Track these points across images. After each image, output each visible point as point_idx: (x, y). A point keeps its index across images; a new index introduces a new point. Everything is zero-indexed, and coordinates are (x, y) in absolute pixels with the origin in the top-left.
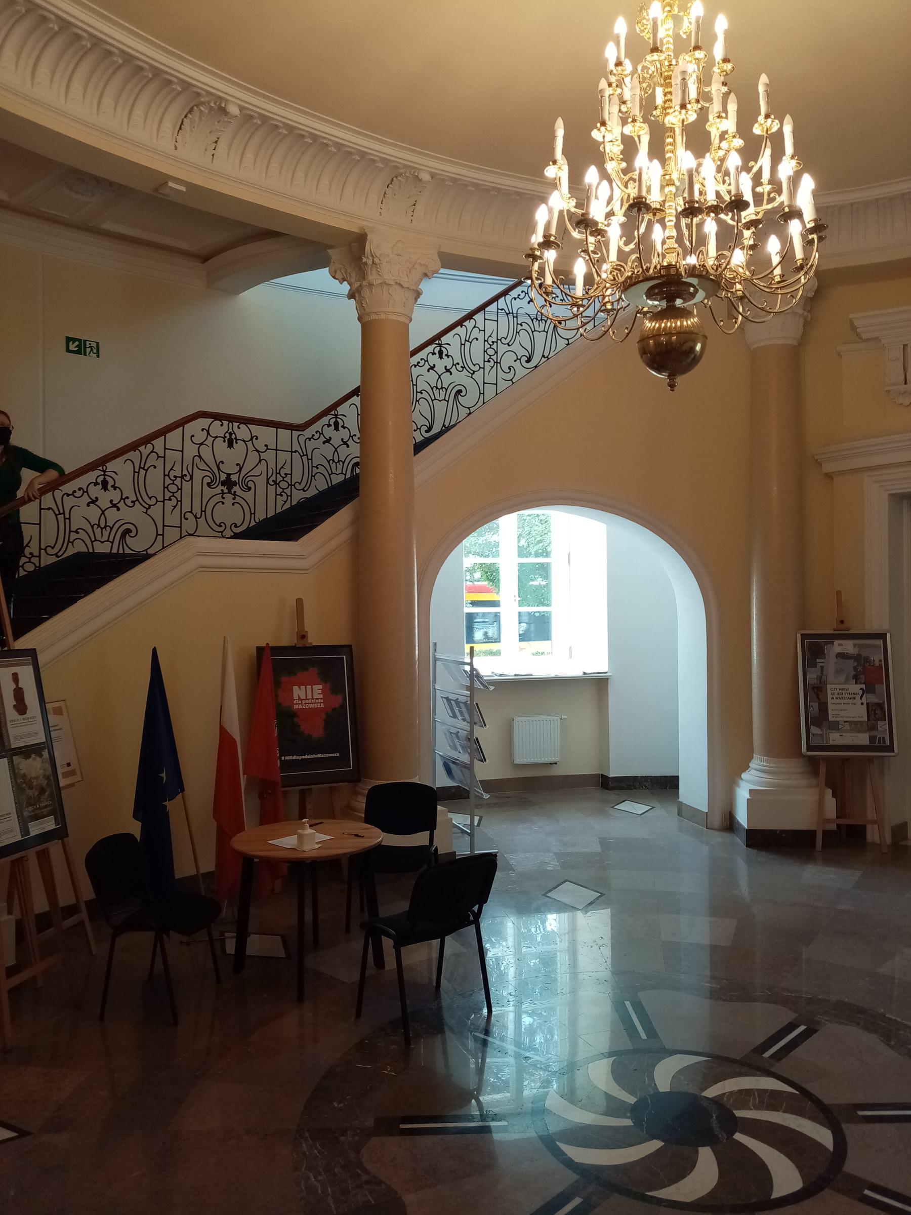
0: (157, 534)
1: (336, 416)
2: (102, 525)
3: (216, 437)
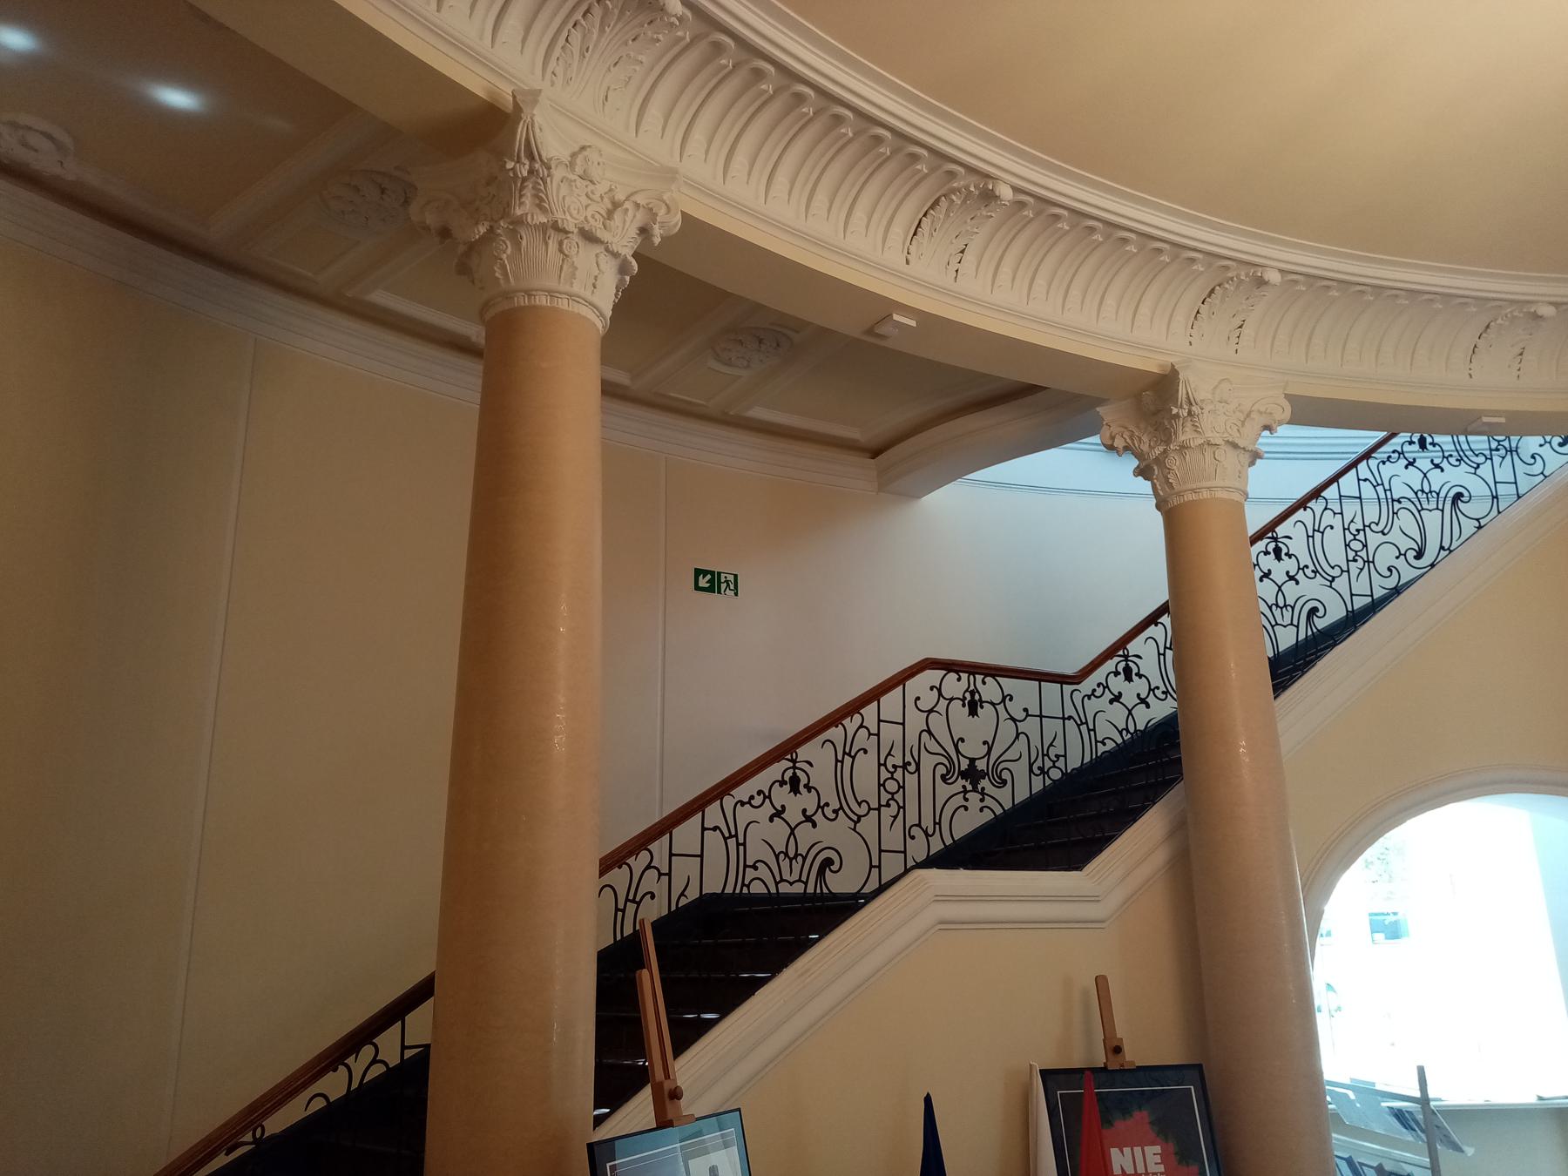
0: (871, 866)
1: (1126, 657)
2: (791, 854)
3: (952, 699)
